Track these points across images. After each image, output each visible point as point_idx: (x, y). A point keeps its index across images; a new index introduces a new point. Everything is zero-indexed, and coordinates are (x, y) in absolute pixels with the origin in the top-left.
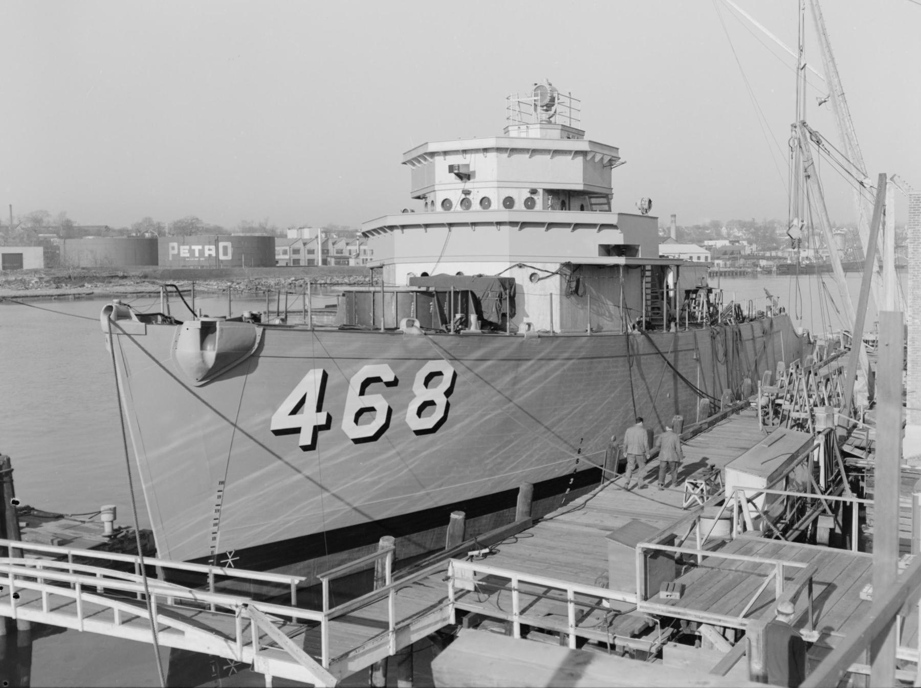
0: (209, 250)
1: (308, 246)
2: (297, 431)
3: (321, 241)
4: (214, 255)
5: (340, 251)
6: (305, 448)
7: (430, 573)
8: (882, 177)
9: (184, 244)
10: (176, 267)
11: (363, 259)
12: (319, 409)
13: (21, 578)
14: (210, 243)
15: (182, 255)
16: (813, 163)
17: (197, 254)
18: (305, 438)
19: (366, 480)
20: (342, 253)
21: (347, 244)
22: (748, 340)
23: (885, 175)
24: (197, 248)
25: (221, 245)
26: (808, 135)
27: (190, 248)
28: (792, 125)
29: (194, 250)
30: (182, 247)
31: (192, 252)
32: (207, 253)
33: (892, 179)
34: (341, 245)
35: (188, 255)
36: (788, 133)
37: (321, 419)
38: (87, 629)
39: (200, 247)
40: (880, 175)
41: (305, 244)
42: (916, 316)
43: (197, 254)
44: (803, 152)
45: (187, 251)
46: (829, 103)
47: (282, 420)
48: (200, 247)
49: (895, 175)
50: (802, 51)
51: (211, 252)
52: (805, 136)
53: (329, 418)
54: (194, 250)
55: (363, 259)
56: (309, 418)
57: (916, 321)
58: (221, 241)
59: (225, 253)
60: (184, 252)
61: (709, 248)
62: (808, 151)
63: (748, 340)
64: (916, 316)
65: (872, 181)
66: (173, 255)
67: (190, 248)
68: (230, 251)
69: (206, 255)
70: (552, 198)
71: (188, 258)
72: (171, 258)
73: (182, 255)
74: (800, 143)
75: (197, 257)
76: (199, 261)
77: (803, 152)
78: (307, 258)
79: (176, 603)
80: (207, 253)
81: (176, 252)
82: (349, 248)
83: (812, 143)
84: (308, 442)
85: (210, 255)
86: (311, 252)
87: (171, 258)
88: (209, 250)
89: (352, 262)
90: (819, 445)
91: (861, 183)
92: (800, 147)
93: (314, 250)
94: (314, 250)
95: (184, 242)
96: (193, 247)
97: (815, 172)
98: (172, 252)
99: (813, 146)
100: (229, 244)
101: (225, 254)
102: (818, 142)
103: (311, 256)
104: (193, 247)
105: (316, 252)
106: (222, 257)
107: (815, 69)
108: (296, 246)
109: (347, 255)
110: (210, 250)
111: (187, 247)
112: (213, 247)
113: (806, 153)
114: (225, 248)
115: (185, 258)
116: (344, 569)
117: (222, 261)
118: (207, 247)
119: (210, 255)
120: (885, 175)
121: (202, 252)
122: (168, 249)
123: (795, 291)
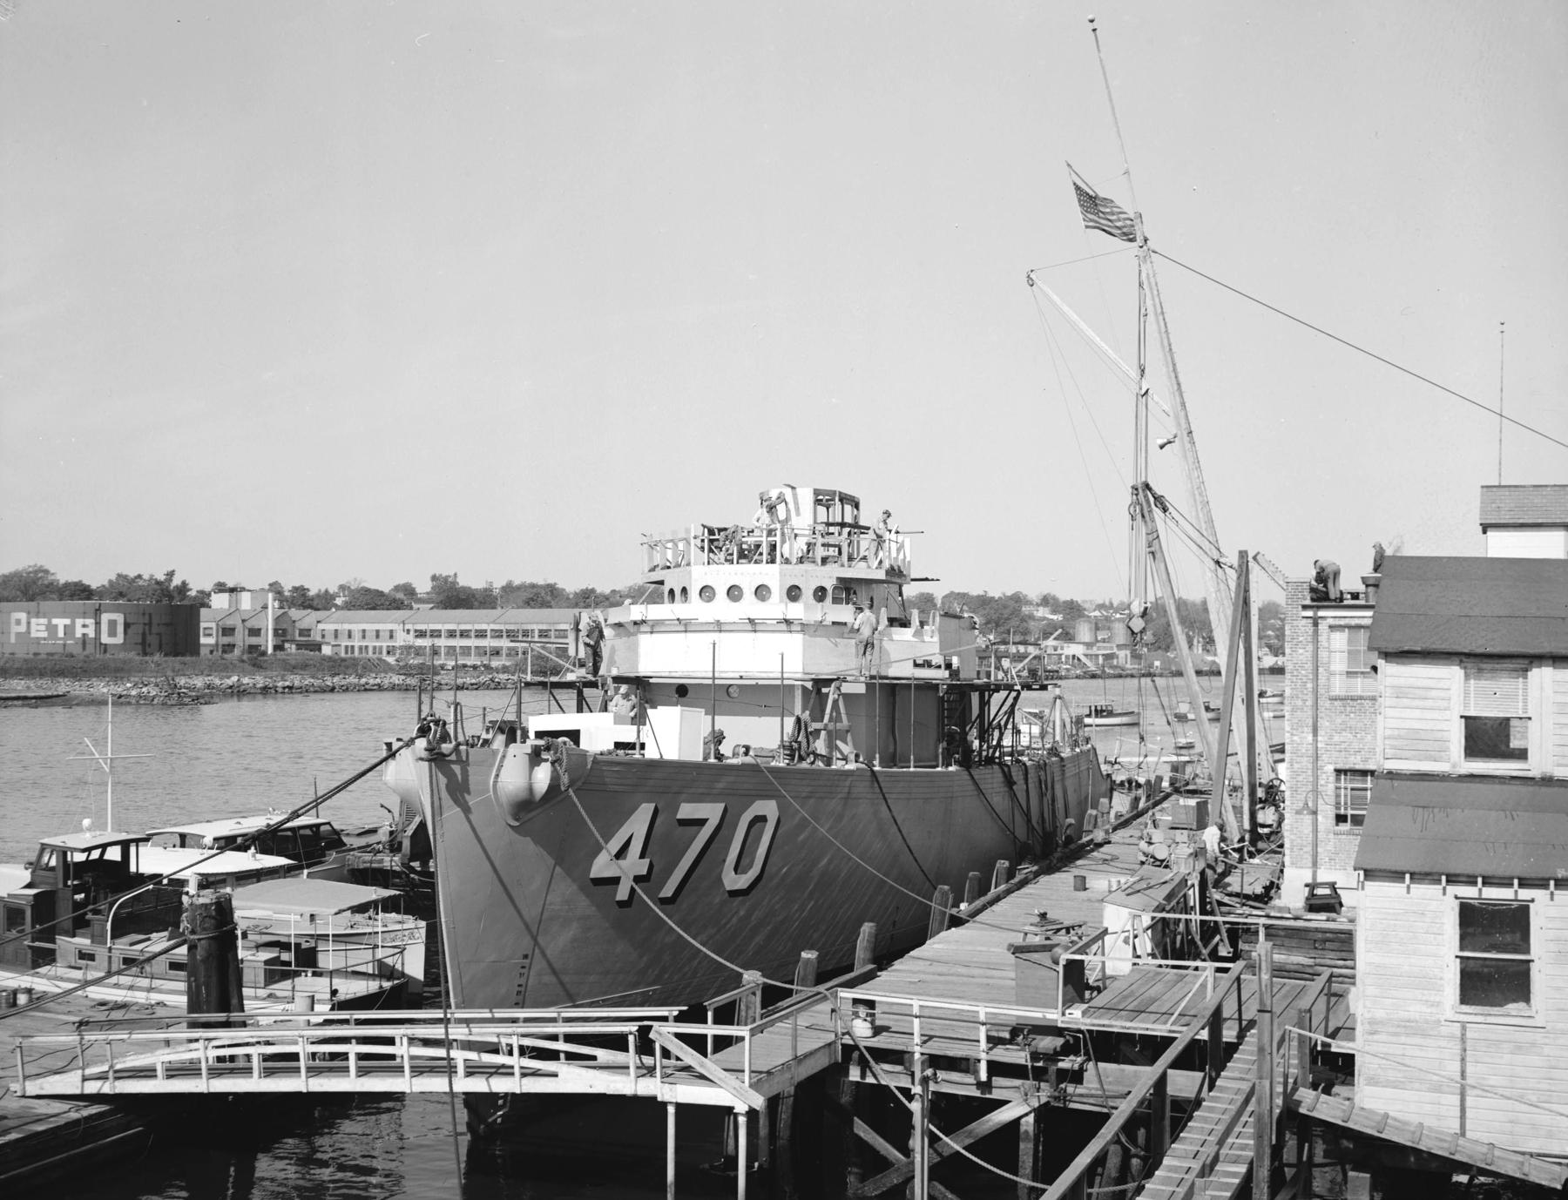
0: (84, 627)
1: (249, 624)
3: (273, 614)
4: (92, 634)
6: (621, 904)
8: (1243, 555)
9: (38, 615)
10: (21, 653)
11: (347, 647)
13: (354, 1041)
14: (84, 616)
15: (34, 634)
16: (1158, 537)
20: (309, 636)
23: (1246, 552)
24: (60, 623)
25: (105, 617)
26: (1152, 500)
27: (50, 622)
28: (1133, 487)
30: (34, 621)
31: (52, 629)
32: (79, 632)
33: (1255, 558)
35: (45, 634)
36: (1128, 498)
38: (526, 1090)
39: (67, 621)
40: (1240, 552)
41: (243, 621)
42: (1295, 732)
43: (61, 634)
44: (1145, 522)
45: (43, 628)
46: (1175, 446)
48: (67, 621)
49: (1258, 553)
50: (1143, 371)
51: (85, 631)
52: (1148, 501)
54: (56, 626)
55: (347, 647)
57: (1295, 738)
58: (105, 612)
60: (39, 628)
62: (1153, 521)
64: (1295, 732)
65: (1233, 559)
66: (18, 634)
67: (50, 622)
69: (78, 634)
71: (45, 639)
72: (13, 640)
73: (34, 634)
74: (1142, 510)
75: (60, 639)
76: (65, 645)
77: (1145, 522)
78: (247, 643)
79: (218, 1062)
80: (79, 632)
81: (23, 628)
82: (321, 626)
83: (1157, 509)
86: (255, 632)
87: (13, 640)
88: (84, 627)
89: (327, 650)
90: (1193, 886)
91: (1218, 562)
92: (1143, 516)
93: (260, 630)
94: (260, 630)
95: (38, 612)
96: (55, 621)
97: (1161, 547)
98: (15, 629)
99: (1157, 512)
101: (112, 633)
102: (1165, 510)
103: (254, 641)
104: (55, 621)
106: (105, 639)
107: (1162, 399)
108: (229, 622)
109: (319, 639)
110: (84, 626)
111: (44, 621)
112: (90, 622)
113: (1149, 523)
114: (112, 624)
116: (425, 1021)
118: (79, 622)
120: (1246, 552)
121: (69, 630)
122: (9, 623)
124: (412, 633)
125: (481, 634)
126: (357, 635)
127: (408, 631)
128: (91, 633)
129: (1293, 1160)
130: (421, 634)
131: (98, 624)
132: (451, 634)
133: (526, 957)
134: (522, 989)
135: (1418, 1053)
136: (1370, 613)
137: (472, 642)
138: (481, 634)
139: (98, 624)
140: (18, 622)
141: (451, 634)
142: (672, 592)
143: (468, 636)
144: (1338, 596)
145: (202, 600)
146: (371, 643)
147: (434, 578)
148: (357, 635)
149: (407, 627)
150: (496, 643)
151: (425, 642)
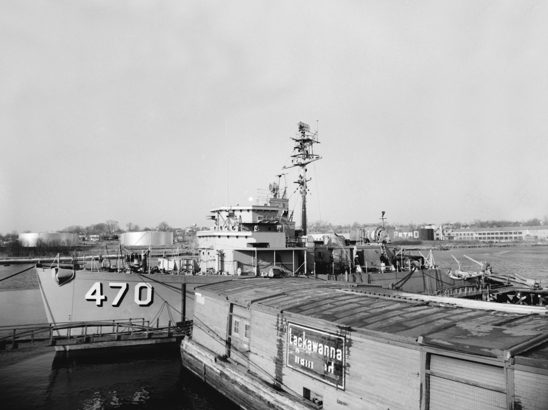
0: (410, 234)
2: (95, 300)
5: (449, 234)
6: (98, 306)
7: (287, 307)
10: (397, 240)
12: (102, 294)
14: (410, 232)
17: (405, 236)
18: (98, 302)
19: (321, 292)
21: (452, 231)
22: (129, 329)
24: (405, 233)
29: (404, 234)
30: (399, 233)
31: (403, 235)
32: (409, 236)
34: (450, 231)
37: (103, 297)
39: (407, 233)
43: (405, 236)
47: (89, 296)
51: (411, 235)
53: (106, 297)
56: (98, 297)
59: (416, 235)
60: (400, 235)
61: (545, 298)
63: (129, 329)
66: (396, 236)
68: (418, 235)
70: (534, 353)
72: (395, 237)
81: (397, 235)
82: (453, 233)
84: (99, 304)
85: (410, 236)
88: (410, 234)
89: (455, 239)
96: (404, 233)
98: (395, 235)
100: (418, 232)
101: (416, 235)
105: (439, 235)
106: (415, 237)
111: (401, 233)
114: (416, 233)
115: (400, 237)
117: (415, 239)
118: (409, 233)
119: (410, 236)
121: (407, 235)
123: (485, 360)
124: (478, 234)
125: (497, 234)
126: (463, 235)
127: (477, 233)
128: (412, 236)
129: (127, 328)
130: (480, 234)
131: (413, 233)
132: (488, 234)
133: (70, 316)
134: (71, 317)
135: (527, 251)
136: (298, 362)
137: (495, 236)
138: (497, 234)
139: (413, 233)
140: (396, 234)
141: (488, 234)
142: (221, 227)
143: (516, 234)
144: (389, 231)
145: (185, 231)
146: (466, 236)
147: (475, 220)
148: (463, 235)
149: (476, 232)
150: (502, 236)
151: (482, 236)
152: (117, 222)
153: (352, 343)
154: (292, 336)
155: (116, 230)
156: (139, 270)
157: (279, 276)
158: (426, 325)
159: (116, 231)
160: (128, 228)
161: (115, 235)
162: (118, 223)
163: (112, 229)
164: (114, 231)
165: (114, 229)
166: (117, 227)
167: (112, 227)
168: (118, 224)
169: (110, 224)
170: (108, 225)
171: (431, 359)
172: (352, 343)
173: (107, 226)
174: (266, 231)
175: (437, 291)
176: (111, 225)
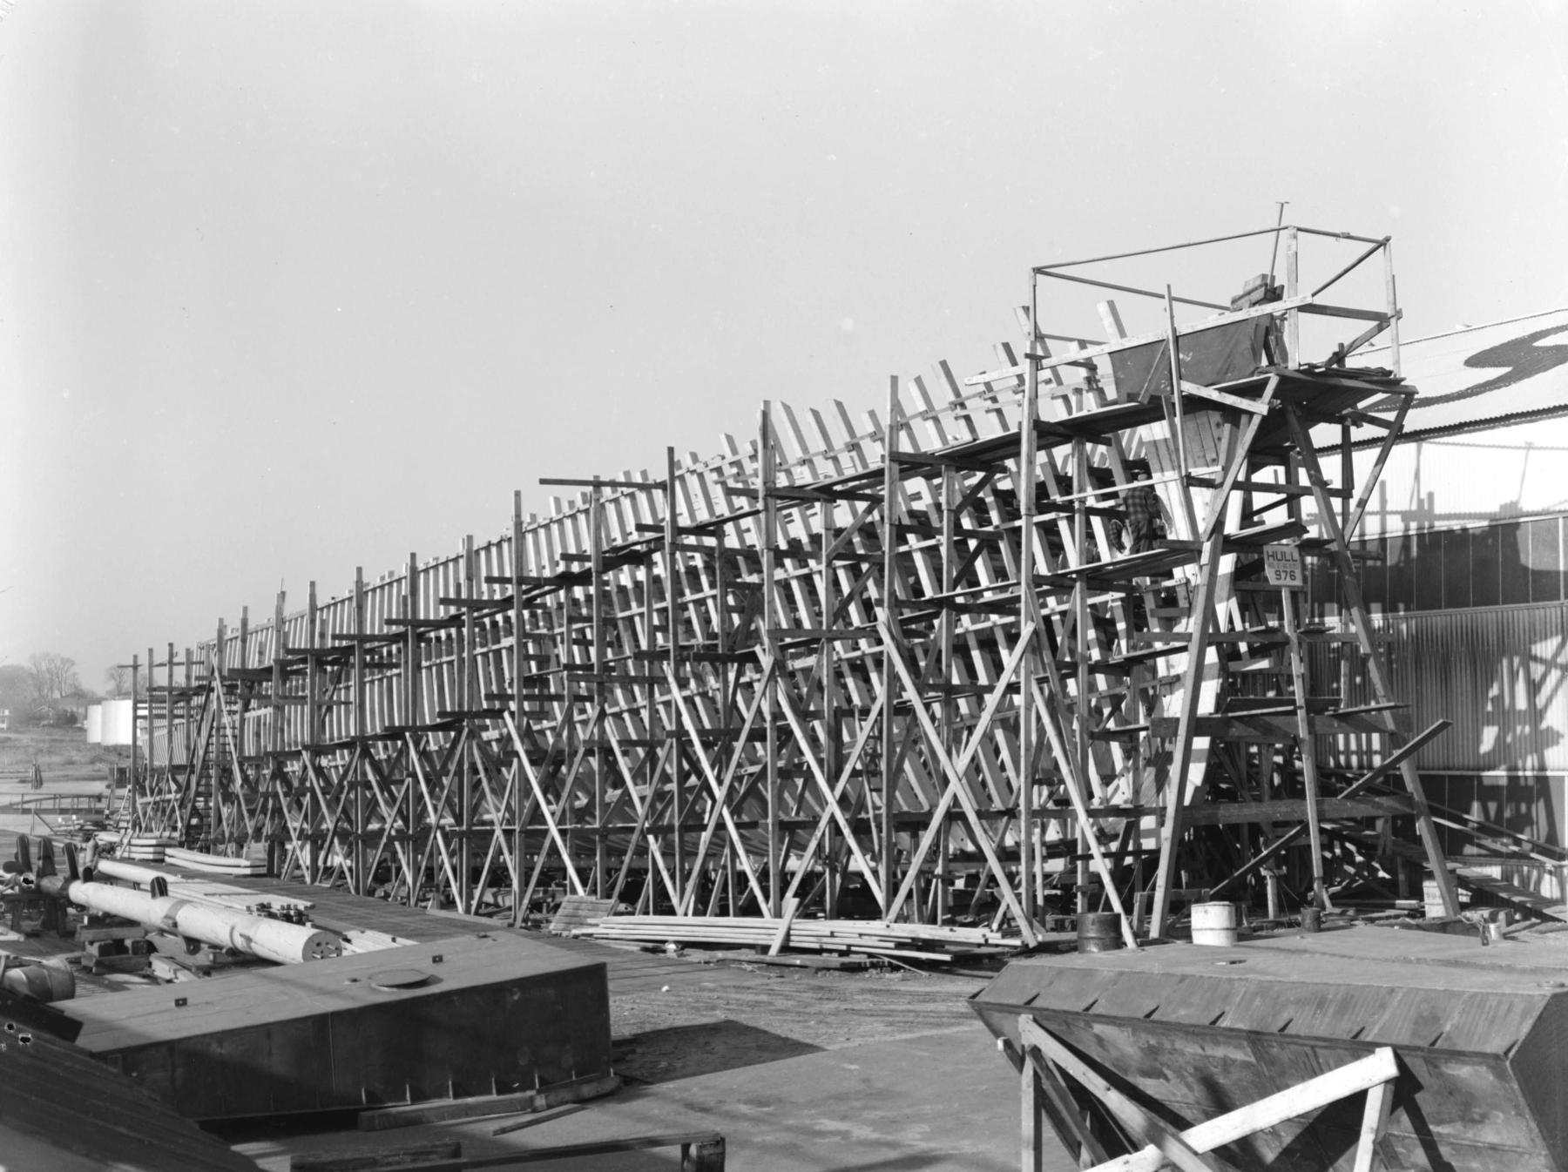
152: (68, 660)
153: (1403, 380)
154: (1282, 626)
155: (67, 690)
156: (786, 795)
157: (284, 623)
158: (1288, 819)
159: (67, 696)
160: (112, 685)
161: (66, 711)
162: (73, 664)
163: (51, 689)
164: (57, 695)
165: (60, 690)
166: (69, 681)
167: (52, 680)
168: (73, 669)
169: (44, 668)
170: (34, 671)
171: (663, 1026)
172: (1403, 380)
173: (31, 674)
174: (180, 1041)
175: (300, 806)
176: (48, 670)
